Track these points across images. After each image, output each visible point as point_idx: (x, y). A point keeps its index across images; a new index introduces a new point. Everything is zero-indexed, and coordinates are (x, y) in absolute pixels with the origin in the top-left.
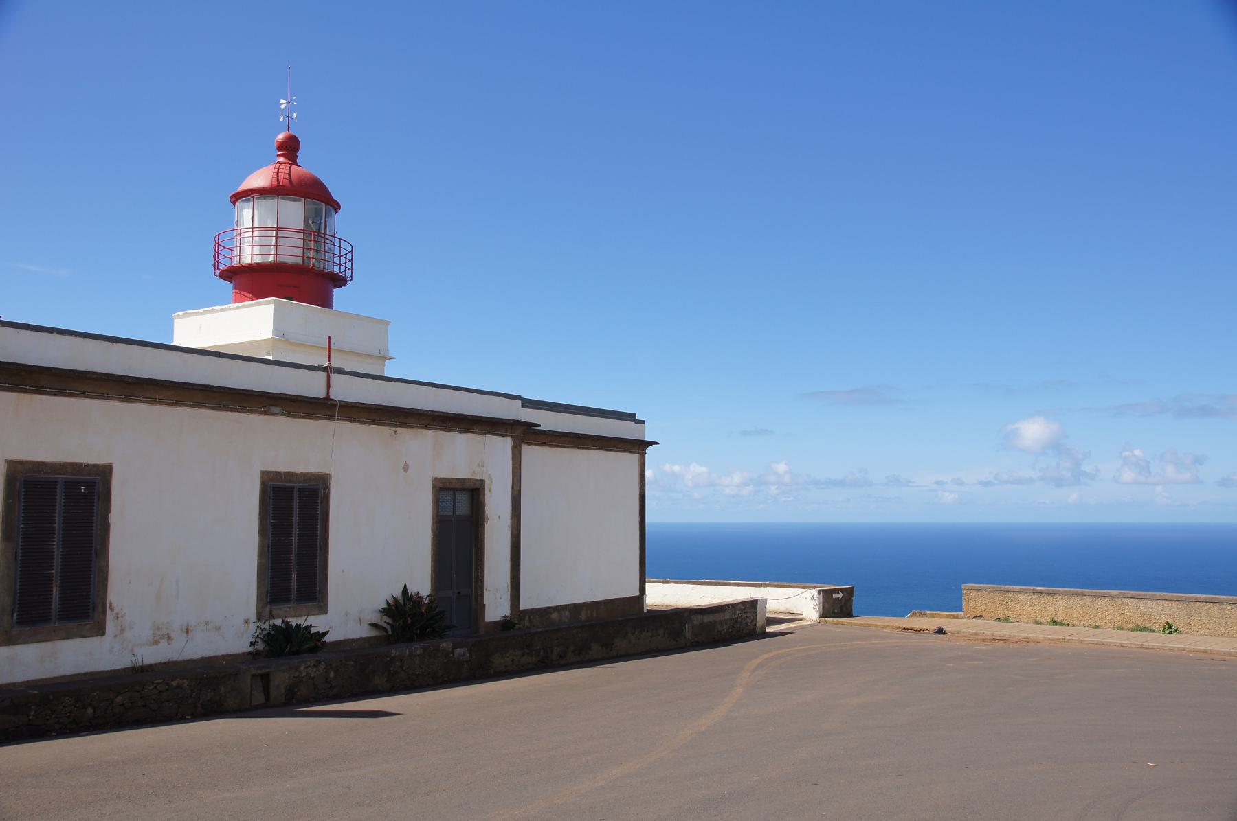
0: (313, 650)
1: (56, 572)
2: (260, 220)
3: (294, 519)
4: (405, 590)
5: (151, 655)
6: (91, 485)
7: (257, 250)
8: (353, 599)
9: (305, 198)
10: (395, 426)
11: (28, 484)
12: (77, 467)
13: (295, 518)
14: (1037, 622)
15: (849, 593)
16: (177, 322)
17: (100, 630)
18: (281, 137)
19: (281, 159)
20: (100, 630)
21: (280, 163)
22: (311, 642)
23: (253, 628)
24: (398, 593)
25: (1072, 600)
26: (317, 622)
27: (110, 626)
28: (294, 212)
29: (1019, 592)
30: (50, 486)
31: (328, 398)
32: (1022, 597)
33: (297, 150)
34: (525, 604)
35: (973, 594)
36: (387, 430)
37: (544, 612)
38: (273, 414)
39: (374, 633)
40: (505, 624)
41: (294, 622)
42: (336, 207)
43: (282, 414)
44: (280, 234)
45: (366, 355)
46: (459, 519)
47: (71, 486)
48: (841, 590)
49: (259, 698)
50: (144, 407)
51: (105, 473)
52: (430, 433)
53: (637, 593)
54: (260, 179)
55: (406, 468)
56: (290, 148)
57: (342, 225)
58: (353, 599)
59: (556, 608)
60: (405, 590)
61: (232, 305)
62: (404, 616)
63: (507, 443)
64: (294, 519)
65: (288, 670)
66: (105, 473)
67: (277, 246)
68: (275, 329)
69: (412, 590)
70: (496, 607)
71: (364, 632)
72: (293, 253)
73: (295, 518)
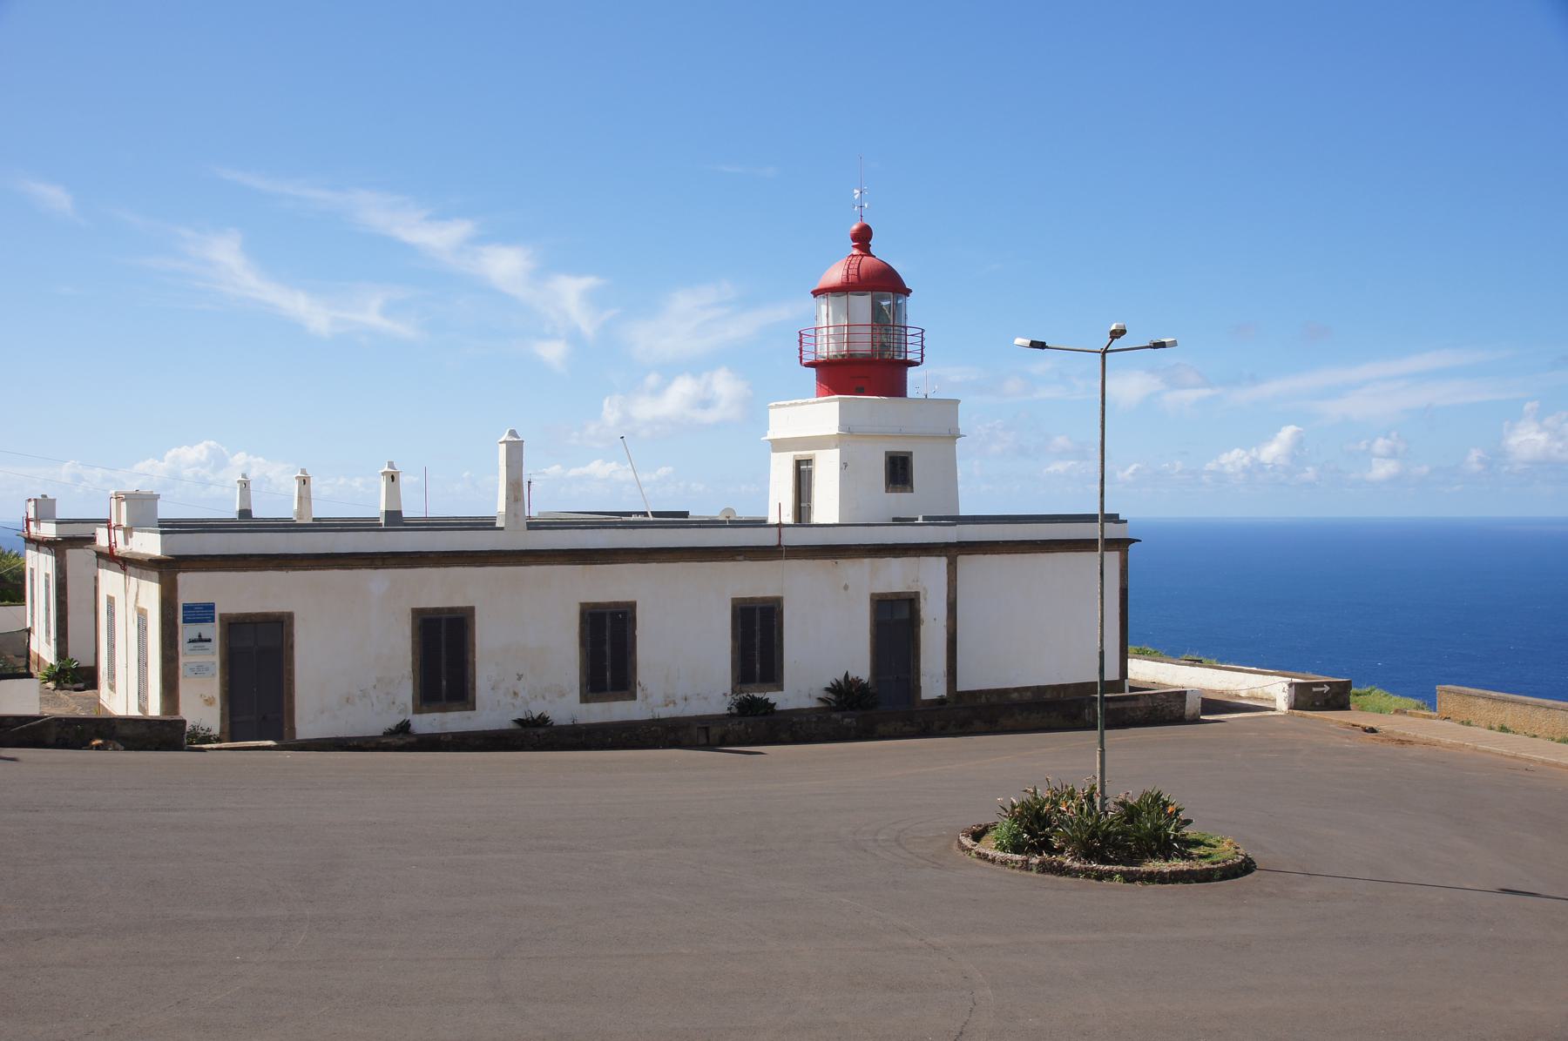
0: (765, 714)
3: (757, 631)
4: (847, 675)
5: (664, 713)
6: (625, 614)
7: (832, 347)
8: (804, 679)
11: (591, 614)
12: (617, 604)
13: (757, 628)
14: (1491, 728)
15: (1346, 686)
16: (771, 411)
17: (634, 697)
18: (855, 227)
19: (856, 252)
20: (634, 697)
22: (768, 707)
23: (729, 698)
24: (841, 678)
25: (1518, 708)
26: (773, 697)
27: (639, 694)
28: (862, 304)
29: (1478, 697)
30: (603, 615)
32: (1481, 702)
34: (962, 686)
35: (1445, 696)
36: (829, 563)
37: (974, 694)
39: (821, 705)
40: (941, 701)
41: (757, 695)
42: (907, 292)
44: (853, 330)
45: (934, 437)
46: (895, 621)
47: (614, 615)
48: (1329, 684)
49: (703, 740)
50: (654, 565)
51: (632, 606)
52: (867, 561)
53: (1117, 678)
55: (846, 588)
56: (863, 237)
57: (915, 311)
58: (804, 679)
59: (1016, 690)
60: (847, 675)
62: (846, 695)
63: (943, 561)
64: (757, 631)
65: (753, 723)
66: (632, 606)
68: (841, 424)
69: (852, 675)
70: (932, 685)
71: (814, 704)
72: (863, 346)
73: (757, 628)
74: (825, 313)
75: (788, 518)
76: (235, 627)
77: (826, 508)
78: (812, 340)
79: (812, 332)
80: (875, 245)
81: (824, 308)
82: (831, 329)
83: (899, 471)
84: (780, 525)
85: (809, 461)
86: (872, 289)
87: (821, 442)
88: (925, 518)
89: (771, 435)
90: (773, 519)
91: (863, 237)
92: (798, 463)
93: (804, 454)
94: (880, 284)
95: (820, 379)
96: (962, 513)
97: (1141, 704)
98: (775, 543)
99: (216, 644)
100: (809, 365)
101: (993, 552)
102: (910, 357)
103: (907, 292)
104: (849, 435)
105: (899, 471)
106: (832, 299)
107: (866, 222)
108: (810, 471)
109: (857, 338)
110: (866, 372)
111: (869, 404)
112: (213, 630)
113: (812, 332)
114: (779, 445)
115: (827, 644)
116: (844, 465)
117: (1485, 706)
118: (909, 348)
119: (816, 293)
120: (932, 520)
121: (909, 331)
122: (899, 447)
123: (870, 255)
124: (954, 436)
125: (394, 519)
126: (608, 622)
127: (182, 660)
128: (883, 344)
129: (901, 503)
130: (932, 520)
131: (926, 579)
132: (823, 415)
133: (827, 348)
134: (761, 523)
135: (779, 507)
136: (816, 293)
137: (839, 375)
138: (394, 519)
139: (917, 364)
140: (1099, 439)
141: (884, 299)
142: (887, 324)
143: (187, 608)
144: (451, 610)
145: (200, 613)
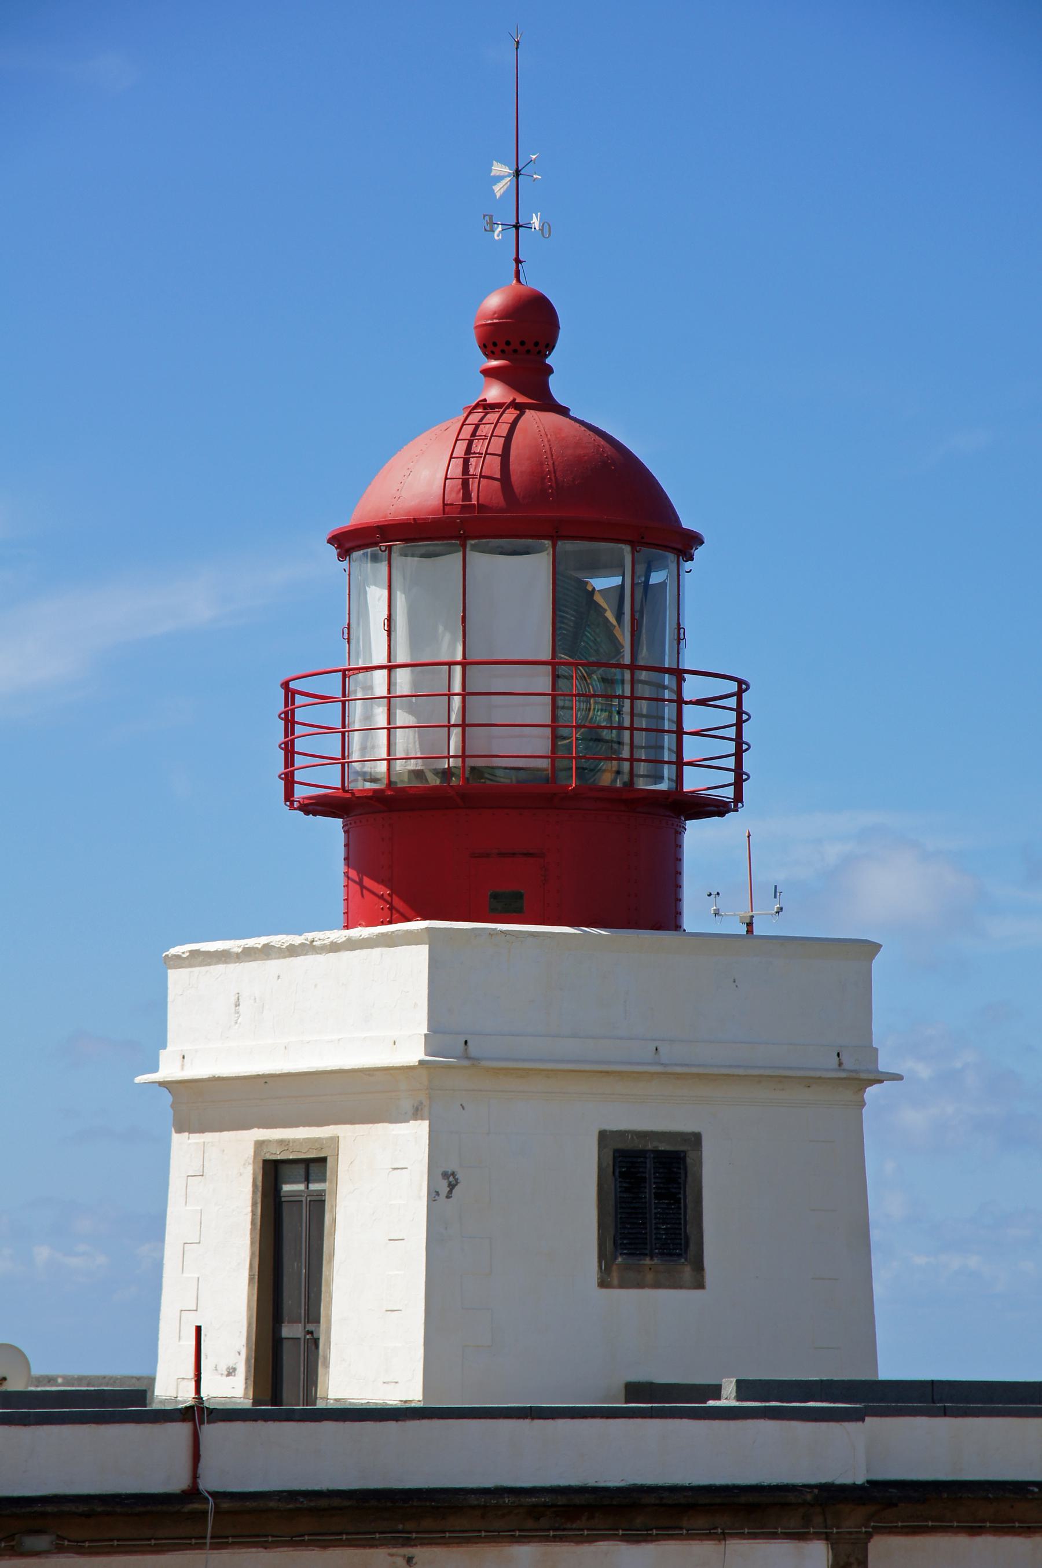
1: (763, 1404)
2: (415, 640)
7: (405, 742)
9: (555, 537)
10: (407, 1542)
16: (175, 976)
18: (494, 301)
19: (495, 392)
21: (486, 406)
28: (518, 587)
31: (193, 1493)
33: (550, 346)
38: (37, 1554)
42: (685, 544)
43: (60, 1549)
45: (780, 1080)
51: (695, 1140)
54: (419, 477)
56: (523, 340)
57: (718, 615)
61: (340, 935)
67: (464, 725)
72: (520, 738)
74: (381, 613)
75: (229, 1384)
77: (376, 1346)
78: (330, 715)
79: (331, 686)
80: (567, 372)
81: (376, 598)
82: (402, 673)
83: (649, 1206)
84: (197, 1414)
85: (315, 1166)
86: (555, 532)
87: (364, 1095)
88: (744, 1388)
89: (169, 1069)
90: (171, 1387)
91: (523, 340)
92: (273, 1173)
93: (297, 1137)
94: (592, 513)
95: (361, 861)
96: (888, 1370)
98: (177, 1482)
100: (320, 806)
102: (694, 781)
103: (685, 544)
104: (459, 1076)
105: (649, 1206)
106: (407, 564)
107: (536, 281)
108: (318, 1205)
109: (501, 710)
110: (531, 836)
111: (550, 962)
113: (331, 686)
114: (206, 1105)
116: (445, 1182)
118: (692, 749)
119: (348, 542)
120: (774, 1398)
121: (693, 688)
122: (650, 1114)
123: (548, 404)
124: (854, 1077)
128: (593, 734)
129: (657, 1327)
130: (774, 1398)
132: (365, 997)
133: (385, 744)
134: (124, 1404)
135: (199, 1334)
136: (348, 542)
137: (424, 848)
139: (716, 808)
140: (524, 1424)
141: (597, 567)
142: (612, 656)
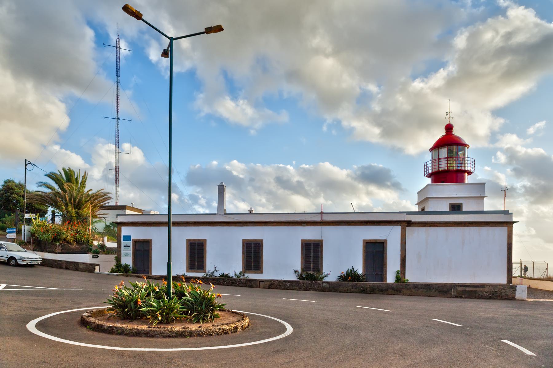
3: (312, 252)
8: (331, 270)
42: (465, 145)
46: (375, 252)
47: (255, 244)
50: (331, 227)
51: (262, 241)
66: (262, 241)
76: (137, 242)
78: (470, 165)
97: (487, 289)
99: (131, 248)
101: (495, 226)
112: (130, 243)
115: (343, 256)
117: (528, 353)
125: (251, 213)
126: (253, 246)
127: (122, 252)
131: (391, 236)
138: (251, 213)
143: (124, 236)
144: (199, 240)
145: (127, 238)
